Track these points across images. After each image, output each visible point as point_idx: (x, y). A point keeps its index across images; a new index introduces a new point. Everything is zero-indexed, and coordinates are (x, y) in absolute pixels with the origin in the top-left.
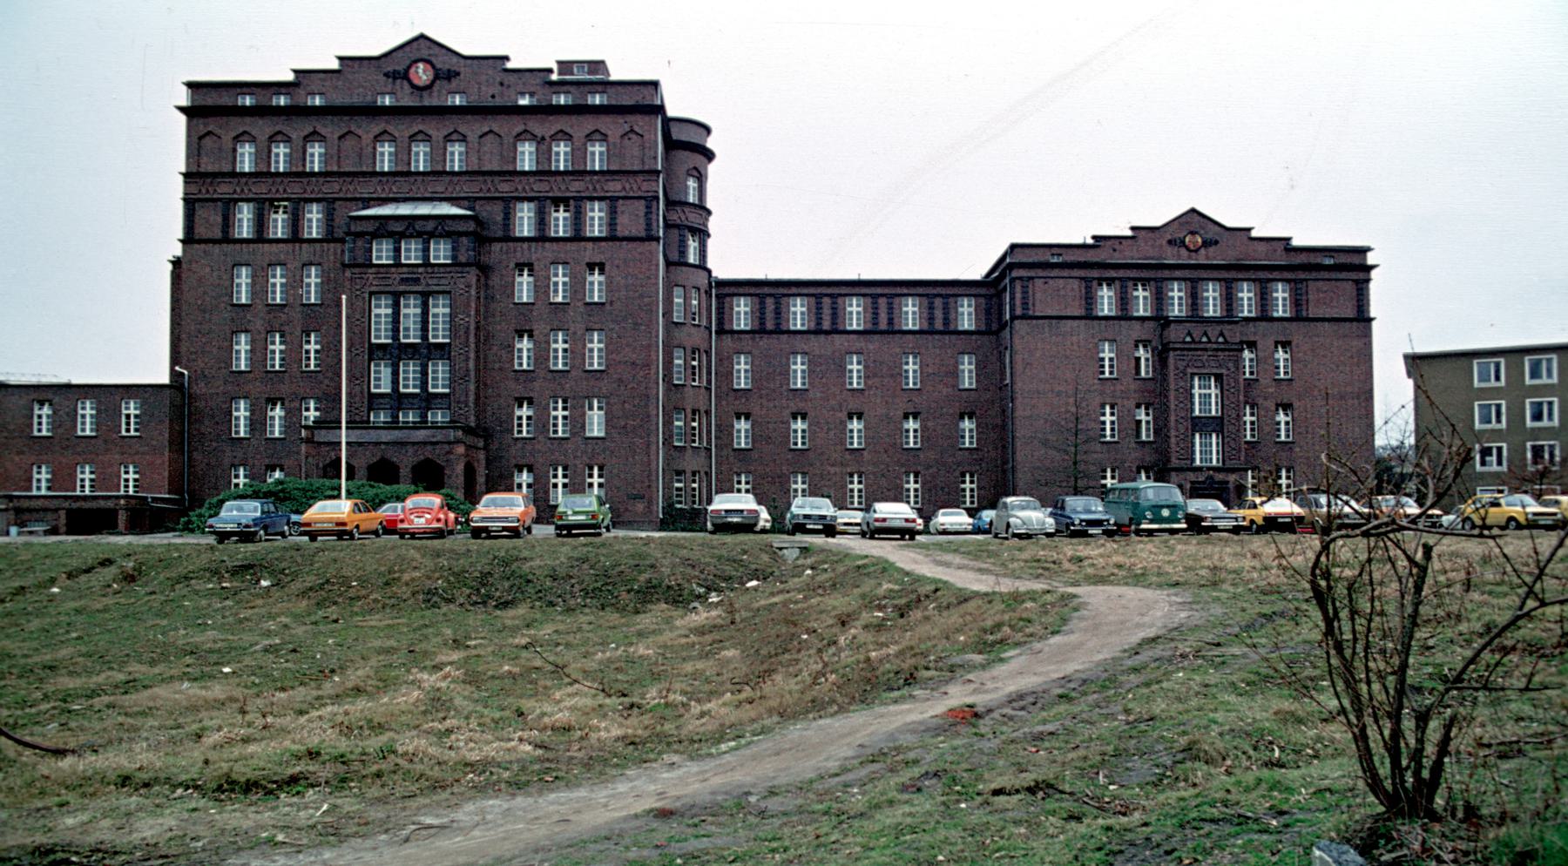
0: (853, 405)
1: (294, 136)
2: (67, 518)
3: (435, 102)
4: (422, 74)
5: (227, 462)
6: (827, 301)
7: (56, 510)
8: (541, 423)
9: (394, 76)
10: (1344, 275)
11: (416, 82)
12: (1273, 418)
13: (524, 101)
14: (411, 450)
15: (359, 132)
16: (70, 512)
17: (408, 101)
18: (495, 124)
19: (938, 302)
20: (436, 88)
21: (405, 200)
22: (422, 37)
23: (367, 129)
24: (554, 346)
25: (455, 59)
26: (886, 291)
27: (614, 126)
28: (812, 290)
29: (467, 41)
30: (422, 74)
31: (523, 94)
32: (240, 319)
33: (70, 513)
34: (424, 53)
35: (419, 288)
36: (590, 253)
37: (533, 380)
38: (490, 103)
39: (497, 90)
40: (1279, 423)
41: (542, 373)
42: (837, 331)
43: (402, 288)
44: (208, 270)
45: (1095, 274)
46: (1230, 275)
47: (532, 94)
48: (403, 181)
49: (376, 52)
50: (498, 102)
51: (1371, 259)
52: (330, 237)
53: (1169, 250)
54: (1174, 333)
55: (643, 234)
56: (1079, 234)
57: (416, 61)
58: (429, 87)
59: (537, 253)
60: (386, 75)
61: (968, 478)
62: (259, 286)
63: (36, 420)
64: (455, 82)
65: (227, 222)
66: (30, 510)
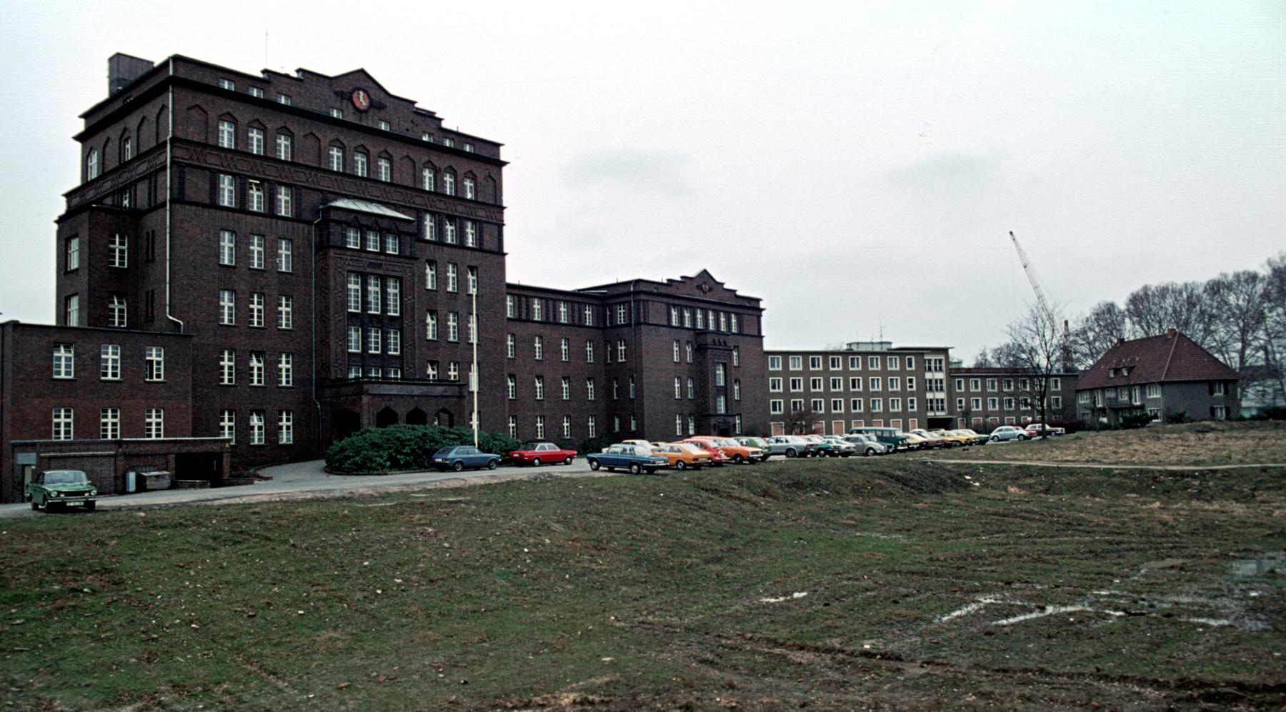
0: (538, 370)
1: (269, 126)
2: (177, 463)
3: (370, 124)
4: (362, 100)
5: (217, 406)
6: (576, 306)
7: (166, 455)
8: (243, 371)
9: (341, 95)
10: (661, 299)
11: (357, 105)
12: (247, 363)
13: (425, 138)
14: (433, 401)
15: (319, 135)
16: (179, 457)
17: (351, 118)
18: (201, 99)
19: (551, 303)
20: (370, 113)
21: (371, 201)
22: (362, 71)
23: (216, 107)
24: (289, 309)
25: (383, 95)
26: (580, 300)
27: (398, 151)
28: (516, 292)
29: (395, 86)
30: (362, 100)
31: (424, 133)
32: (286, 286)
33: (179, 457)
34: (363, 84)
35: (380, 272)
36: (470, 259)
37: (437, 348)
38: (404, 133)
39: (409, 125)
40: (252, 369)
41: (443, 343)
42: (530, 320)
43: (369, 270)
44: (198, 230)
45: (671, 301)
46: (706, 306)
47: (430, 135)
48: (368, 187)
49: (331, 74)
50: (409, 135)
51: (762, 305)
52: (297, 218)
53: (697, 291)
54: (709, 339)
55: (207, 201)
56: (661, 277)
57: (359, 89)
58: (366, 112)
59: (438, 254)
60: (336, 93)
61: (284, 416)
62: (242, 252)
63: (162, 373)
64: (383, 112)
65: (215, 189)
66: (138, 456)
